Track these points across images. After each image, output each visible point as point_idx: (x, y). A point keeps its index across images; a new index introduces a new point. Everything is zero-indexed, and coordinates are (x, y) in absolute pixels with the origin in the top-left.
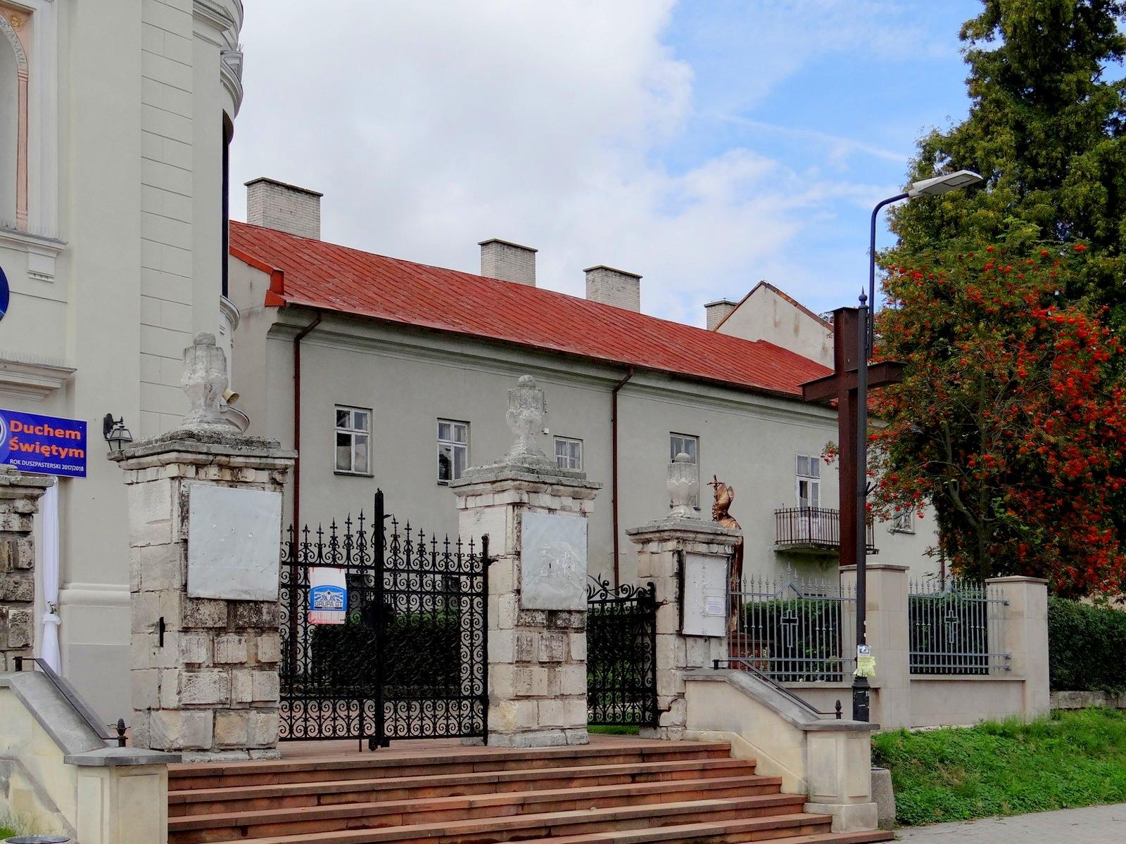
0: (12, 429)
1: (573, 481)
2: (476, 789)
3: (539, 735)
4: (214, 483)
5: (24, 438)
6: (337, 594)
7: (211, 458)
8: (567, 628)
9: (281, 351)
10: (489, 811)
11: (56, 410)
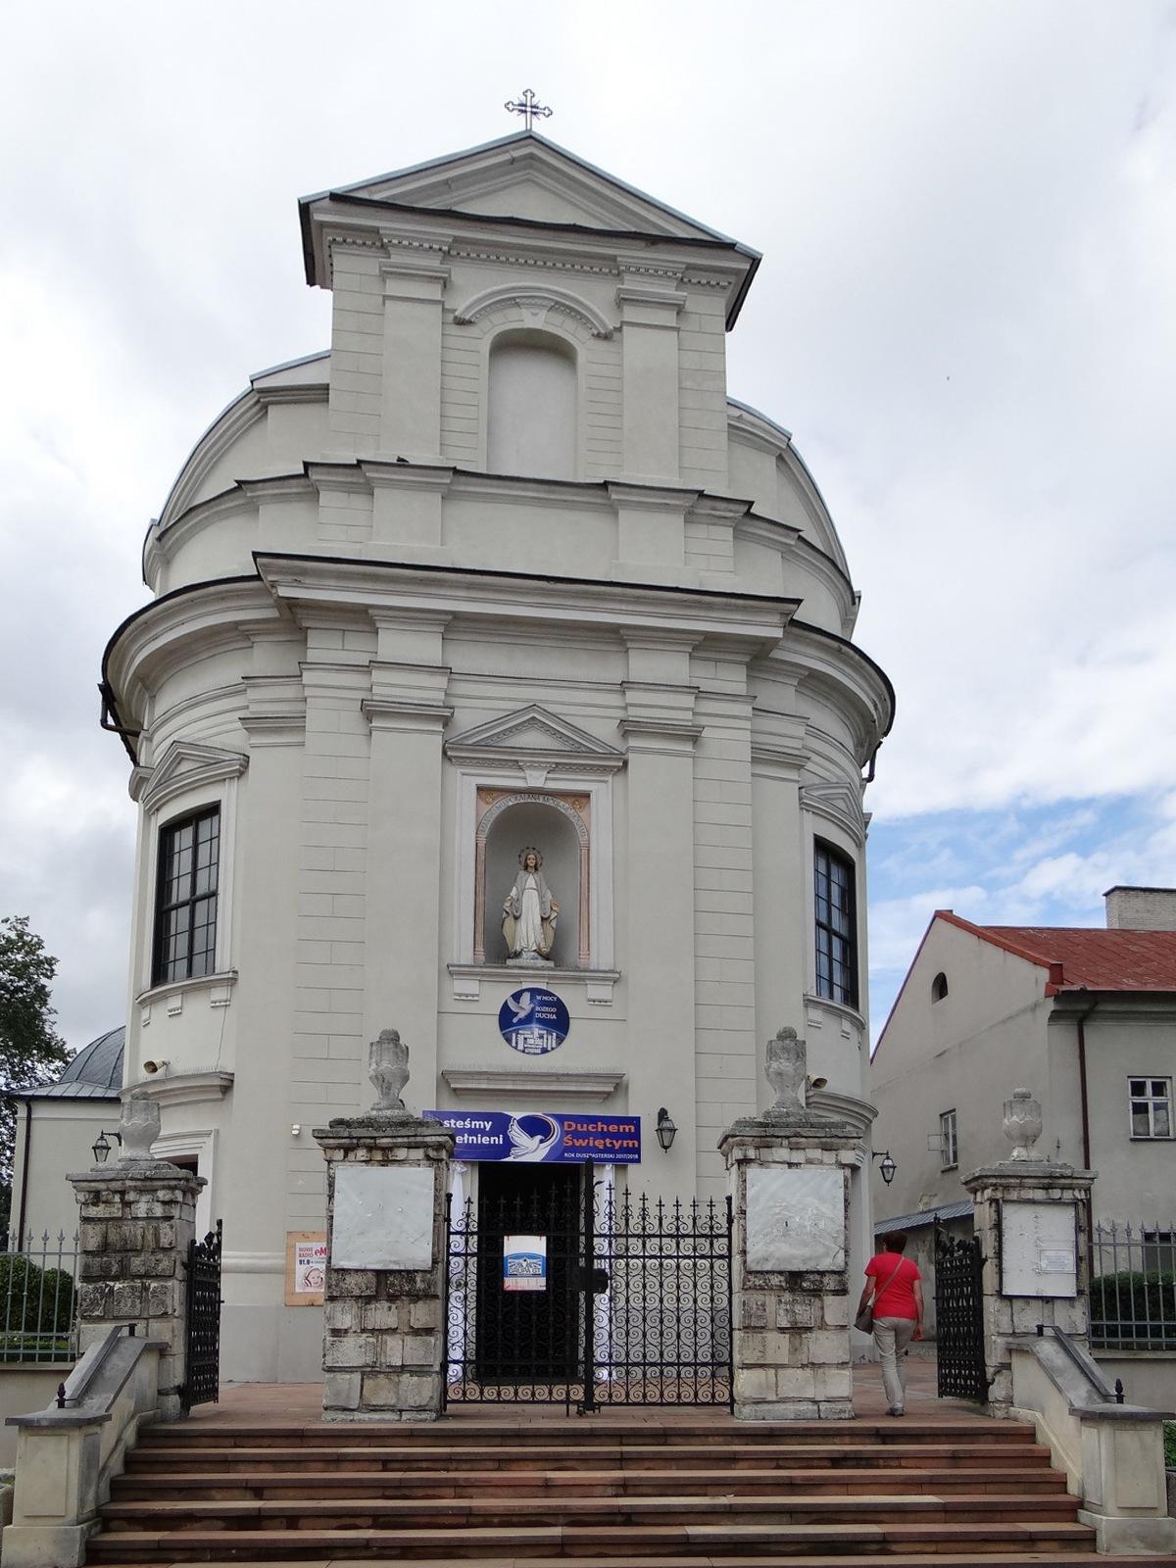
0: (566, 1128)
1: (818, 1132)
2: (591, 1464)
3: (777, 1407)
4: (364, 1164)
5: (576, 1135)
6: (535, 1261)
7: (355, 1141)
8: (820, 1290)
9: (1066, 1036)
10: (575, 1490)
11: (615, 1110)
